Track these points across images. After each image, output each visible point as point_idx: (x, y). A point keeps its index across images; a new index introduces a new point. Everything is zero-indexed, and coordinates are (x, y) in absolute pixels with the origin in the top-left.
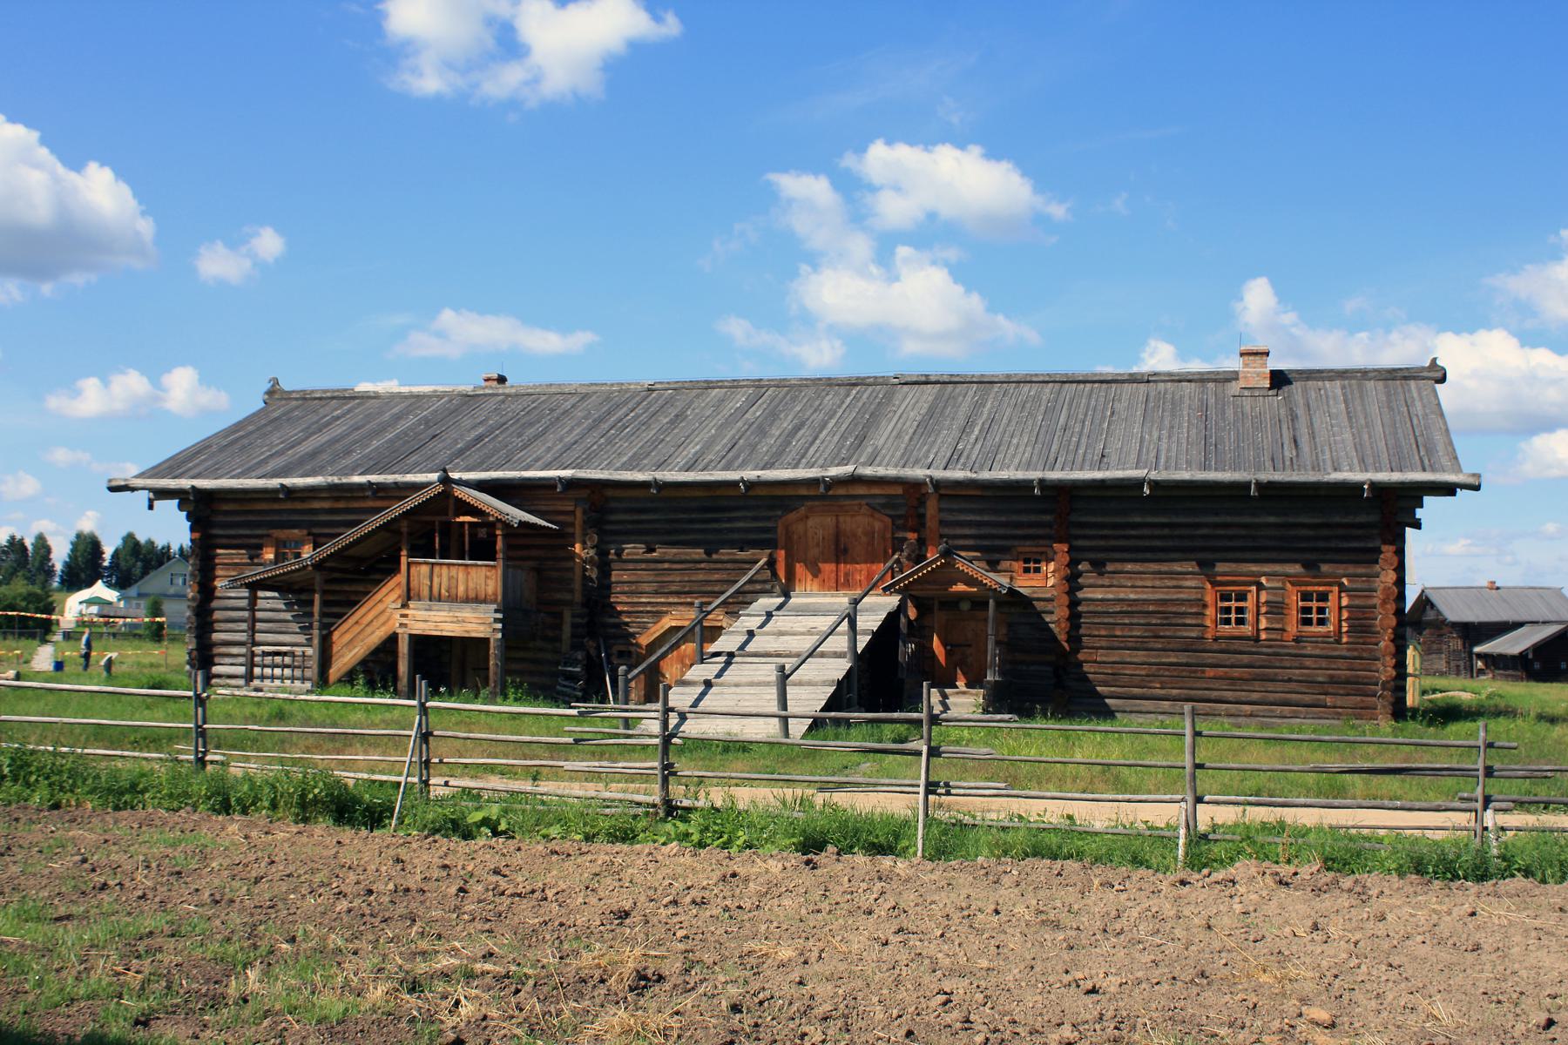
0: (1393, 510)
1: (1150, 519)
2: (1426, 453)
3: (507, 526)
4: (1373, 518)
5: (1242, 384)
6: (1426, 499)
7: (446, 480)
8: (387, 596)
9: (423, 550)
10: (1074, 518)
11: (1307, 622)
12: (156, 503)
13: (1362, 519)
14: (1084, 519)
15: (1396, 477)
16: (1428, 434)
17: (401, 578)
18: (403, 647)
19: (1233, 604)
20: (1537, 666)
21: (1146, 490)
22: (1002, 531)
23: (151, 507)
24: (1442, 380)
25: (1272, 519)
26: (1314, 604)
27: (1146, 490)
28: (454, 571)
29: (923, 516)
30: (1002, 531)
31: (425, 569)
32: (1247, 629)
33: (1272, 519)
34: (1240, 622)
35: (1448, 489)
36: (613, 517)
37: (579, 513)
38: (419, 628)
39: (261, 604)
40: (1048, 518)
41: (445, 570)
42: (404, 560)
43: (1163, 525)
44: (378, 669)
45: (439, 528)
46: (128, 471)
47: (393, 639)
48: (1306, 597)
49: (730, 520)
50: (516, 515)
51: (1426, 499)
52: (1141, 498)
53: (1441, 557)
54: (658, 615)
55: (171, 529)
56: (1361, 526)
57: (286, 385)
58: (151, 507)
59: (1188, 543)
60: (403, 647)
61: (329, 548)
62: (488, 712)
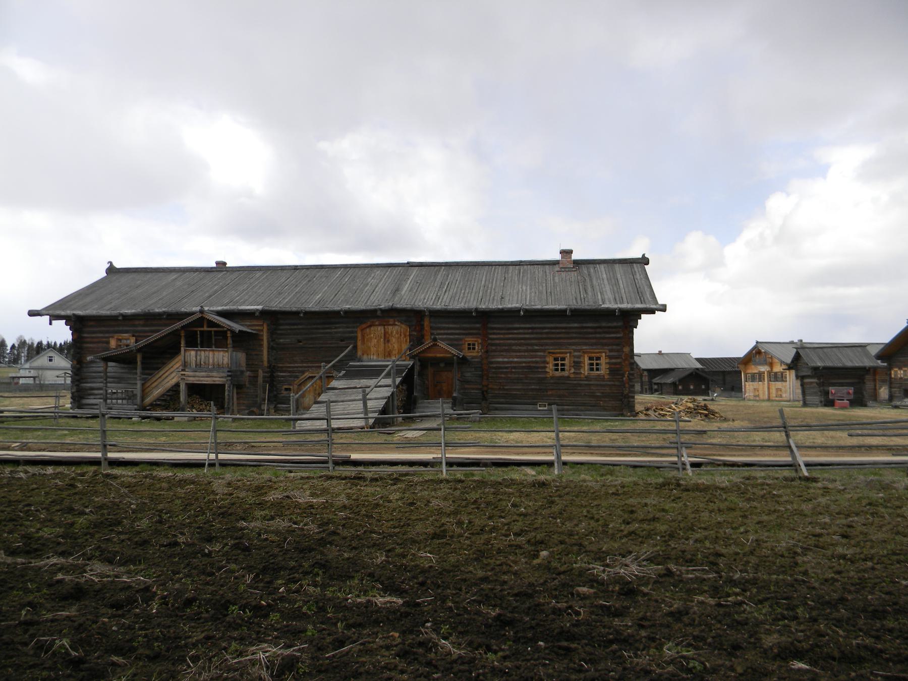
0: (630, 318)
1: (558, 325)
2: (641, 296)
3: (233, 332)
4: (620, 324)
5: (561, 266)
6: (643, 316)
7: (202, 312)
8: (176, 364)
9: (192, 343)
10: (490, 325)
11: (592, 369)
12: (54, 322)
13: (615, 324)
14: (440, 325)
15: (629, 306)
16: (644, 289)
17: (181, 357)
18: (183, 387)
19: (560, 362)
20: (680, 387)
21: (522, 313)
22: (457, 331)
23: (51, 324)
24: (647, 263)
25: (576, 325)
26: (595, 362)
27: (522, 313)
28: (207, 353)
29: (423, 325)
30: (457, 331)
31: (193, 353)
32: (566, 374)
33: (576, 325)
34: (563, 370)
35: (652, 312)
36: (282, 327)
37: (265, 326)
38: (191, 380)
39: (109, 369)
40: (478, 325)
41: (203, 353)
42: (182, 349)
43: (529, 328)
44: (170, 400)
45: (199, 331)
46: (39, 307)
47: (177, 385)
48: (591, 359)
49: (336, 328)
50: (237, 327)
51: (643, 316)
52: (519, 316)
53: (650, 338)
54: (303, 372)
55: (62, 333)
56: (615, 327)
57: (118, 265)
58: (51, 324)
59: (540, 336)
60: (183, 387)
61: (143, 342)
62: (40, 450)
